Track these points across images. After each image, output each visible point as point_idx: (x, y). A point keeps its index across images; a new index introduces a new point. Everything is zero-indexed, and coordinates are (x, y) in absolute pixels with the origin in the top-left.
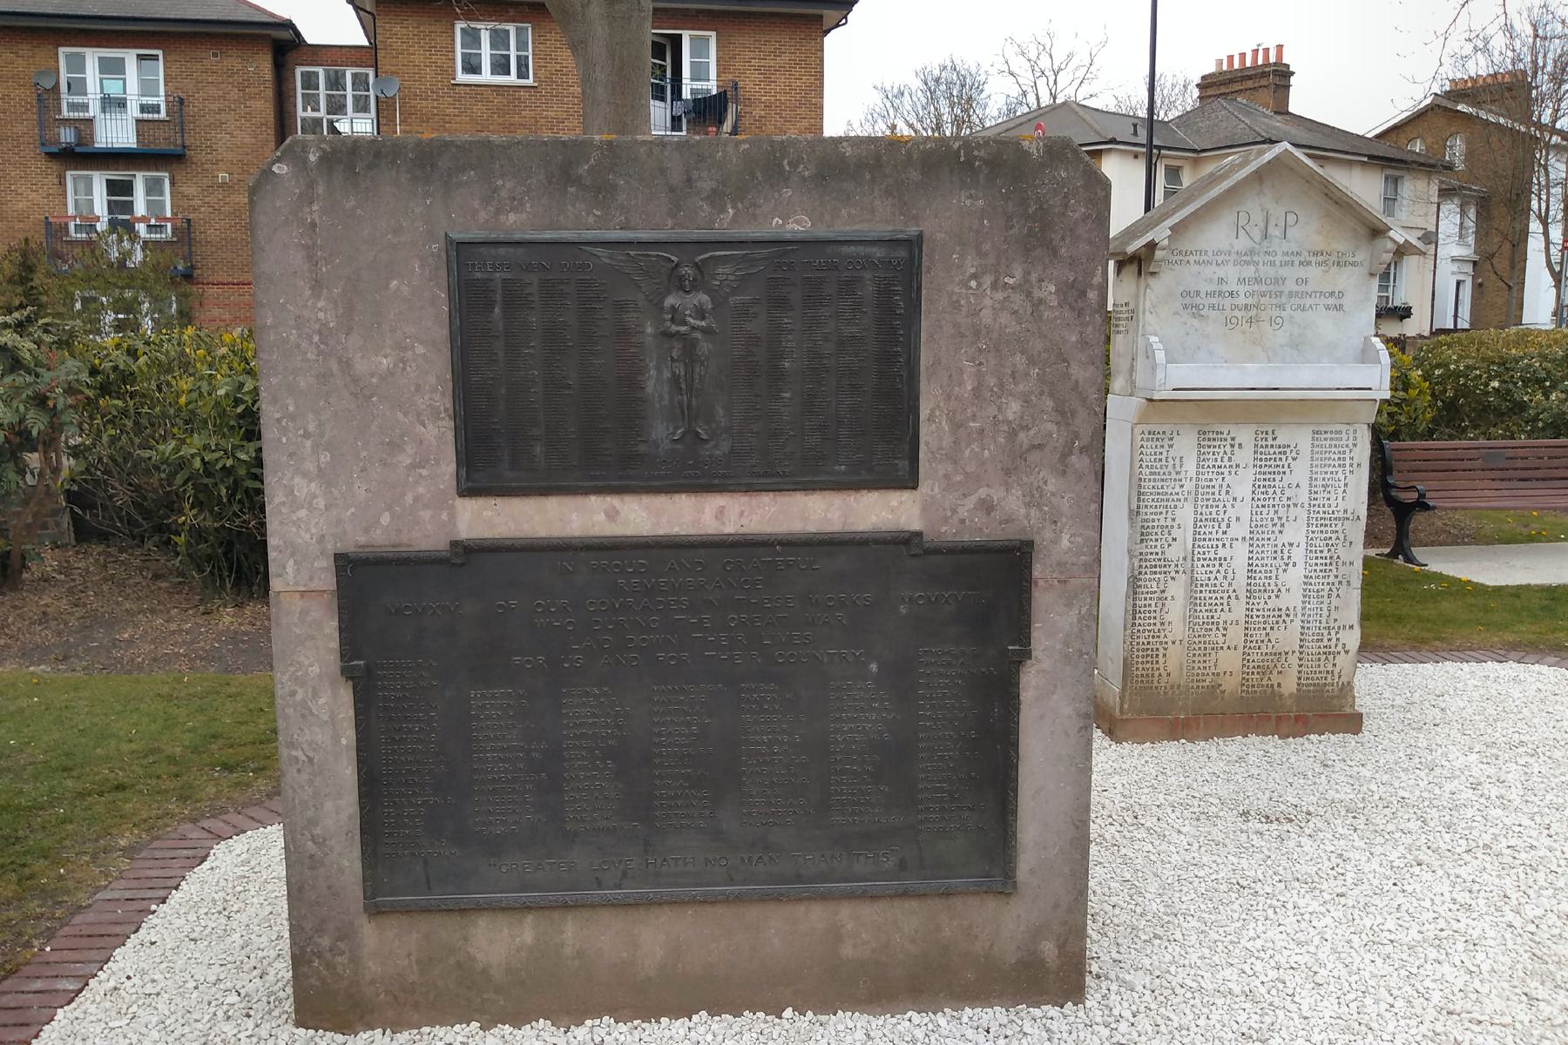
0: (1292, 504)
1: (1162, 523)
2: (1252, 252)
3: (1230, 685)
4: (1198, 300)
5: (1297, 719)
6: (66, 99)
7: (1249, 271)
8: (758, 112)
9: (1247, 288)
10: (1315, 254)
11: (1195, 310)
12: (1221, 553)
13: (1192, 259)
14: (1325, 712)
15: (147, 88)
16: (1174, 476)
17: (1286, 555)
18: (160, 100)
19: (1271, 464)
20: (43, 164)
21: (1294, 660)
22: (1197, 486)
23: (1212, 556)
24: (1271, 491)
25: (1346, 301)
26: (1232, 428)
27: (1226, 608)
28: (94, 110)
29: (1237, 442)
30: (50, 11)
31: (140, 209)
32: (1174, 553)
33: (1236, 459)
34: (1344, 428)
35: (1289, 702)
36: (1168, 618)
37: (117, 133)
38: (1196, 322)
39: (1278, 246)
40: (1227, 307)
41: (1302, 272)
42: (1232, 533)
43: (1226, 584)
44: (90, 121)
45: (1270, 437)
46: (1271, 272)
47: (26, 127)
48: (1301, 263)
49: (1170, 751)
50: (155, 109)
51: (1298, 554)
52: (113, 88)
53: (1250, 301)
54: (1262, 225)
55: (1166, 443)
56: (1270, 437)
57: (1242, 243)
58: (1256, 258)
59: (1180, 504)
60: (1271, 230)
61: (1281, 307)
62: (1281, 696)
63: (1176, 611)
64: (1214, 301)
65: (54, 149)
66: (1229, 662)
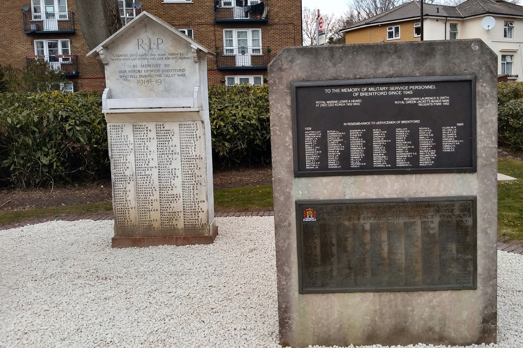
0: (173, 153)
1: (122, 161)
2: (145, 55)
3: (156, 225)
4: (126, 74)
5: (184, 238)
6: (33, 14)
7: (145, 62)
8: (276, 9)
9: (145, 69)
10: (172, 54)
11: (125, 78)
12: (147, 173)
14: (200, 235)
15: (61, 9)
16: (125, 143)
18: (66, 13)
19: (163, 138)
20: (26, 37)
21: (181, 215)
22: (134, 147)
24: (165, 148)
25: (187, 73)
26: (146, 123)
28: (43, 17)
29: (149, 129)
31: (60, 52)
32: (128, 173)
34: (192, 123)
35: (181, 232)
36: (128, 199)
37: (51, 26)
39: (155, 51)
42: (150, 165)
43: (150, 185)
44: (42, 22)
45: (162, 128)
47: (20, 25)
49: (136, 251)
50: (65, 16)
51: (179, 173)
52: (50, 10)
53: (147, 74)
54: (148, 44)
55: (120, 130)
57: (141, 51)
59: (128, 154)
61: (160, 76)
62: (178, 229)
63: (131, 196)
64: (132, 74)
65: (29, 32)
66: (155, 216)
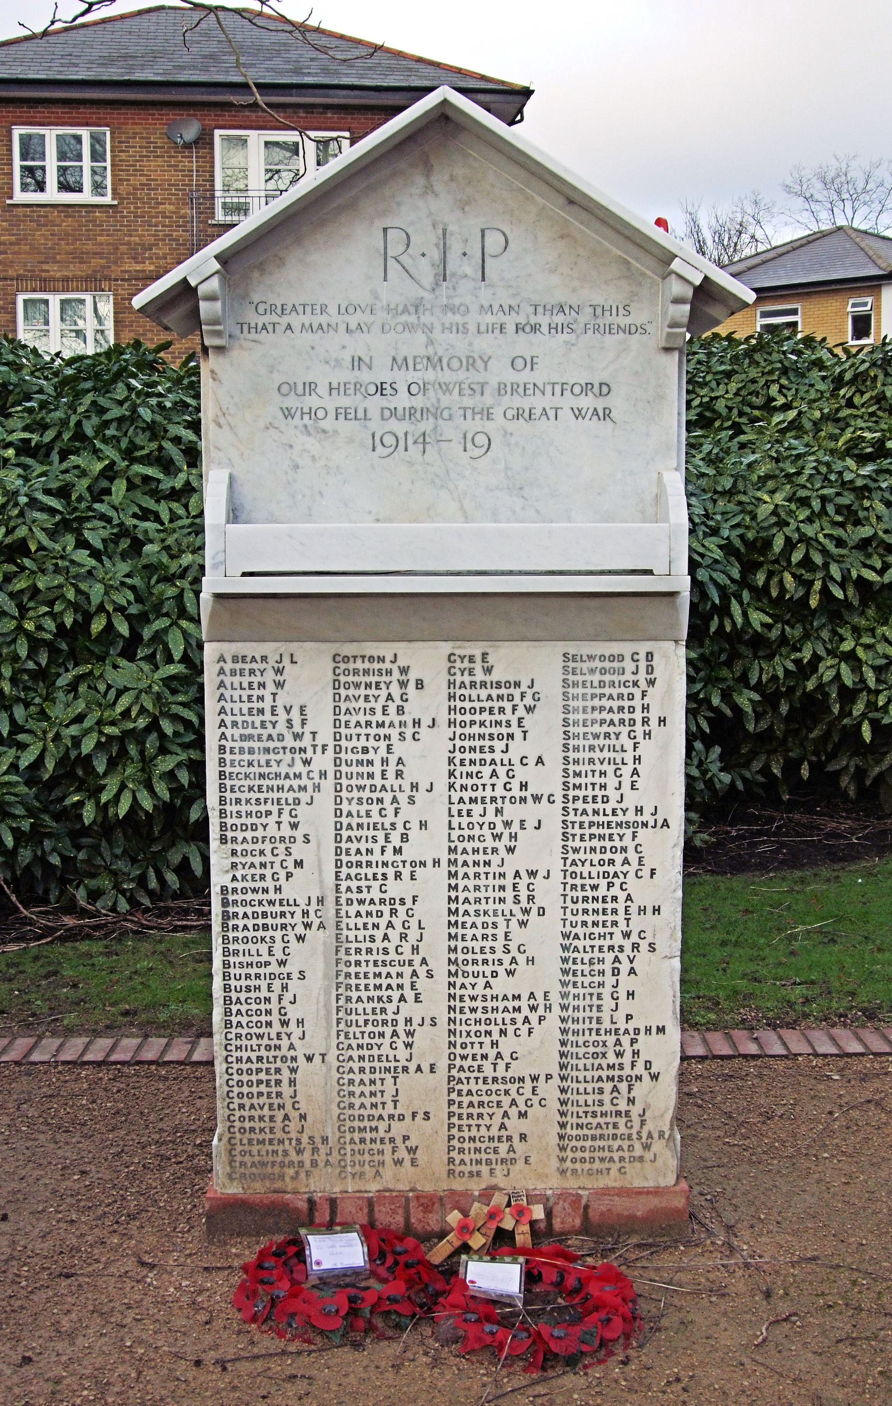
1: (272, 830)
2: (418, 306)
12: (394, 889)
13: (296, 320)
16: (289, 742)
17: (524, 894)
19: (483, 721)
22: (337, 762)
23: (376, 895)
24: (487, 770)
25: (616, 402)
26: (400, 648)
27: (409, 995)
29: (412, 676)
30: (658, 599)
33: (413, 710)
38: (311, 444)
40: (374, 413)
41: (523, 345)
42: (410, 852)
43: (406, 948)
45: (478, 667)
46: (460, 345)
48: (518, 328)
51: (549, 893)
54: (436, 255)
56: (478, 667)
57: (397, 289)
58: (426, 319)
59: (304, 797)
60: (453, 265)
